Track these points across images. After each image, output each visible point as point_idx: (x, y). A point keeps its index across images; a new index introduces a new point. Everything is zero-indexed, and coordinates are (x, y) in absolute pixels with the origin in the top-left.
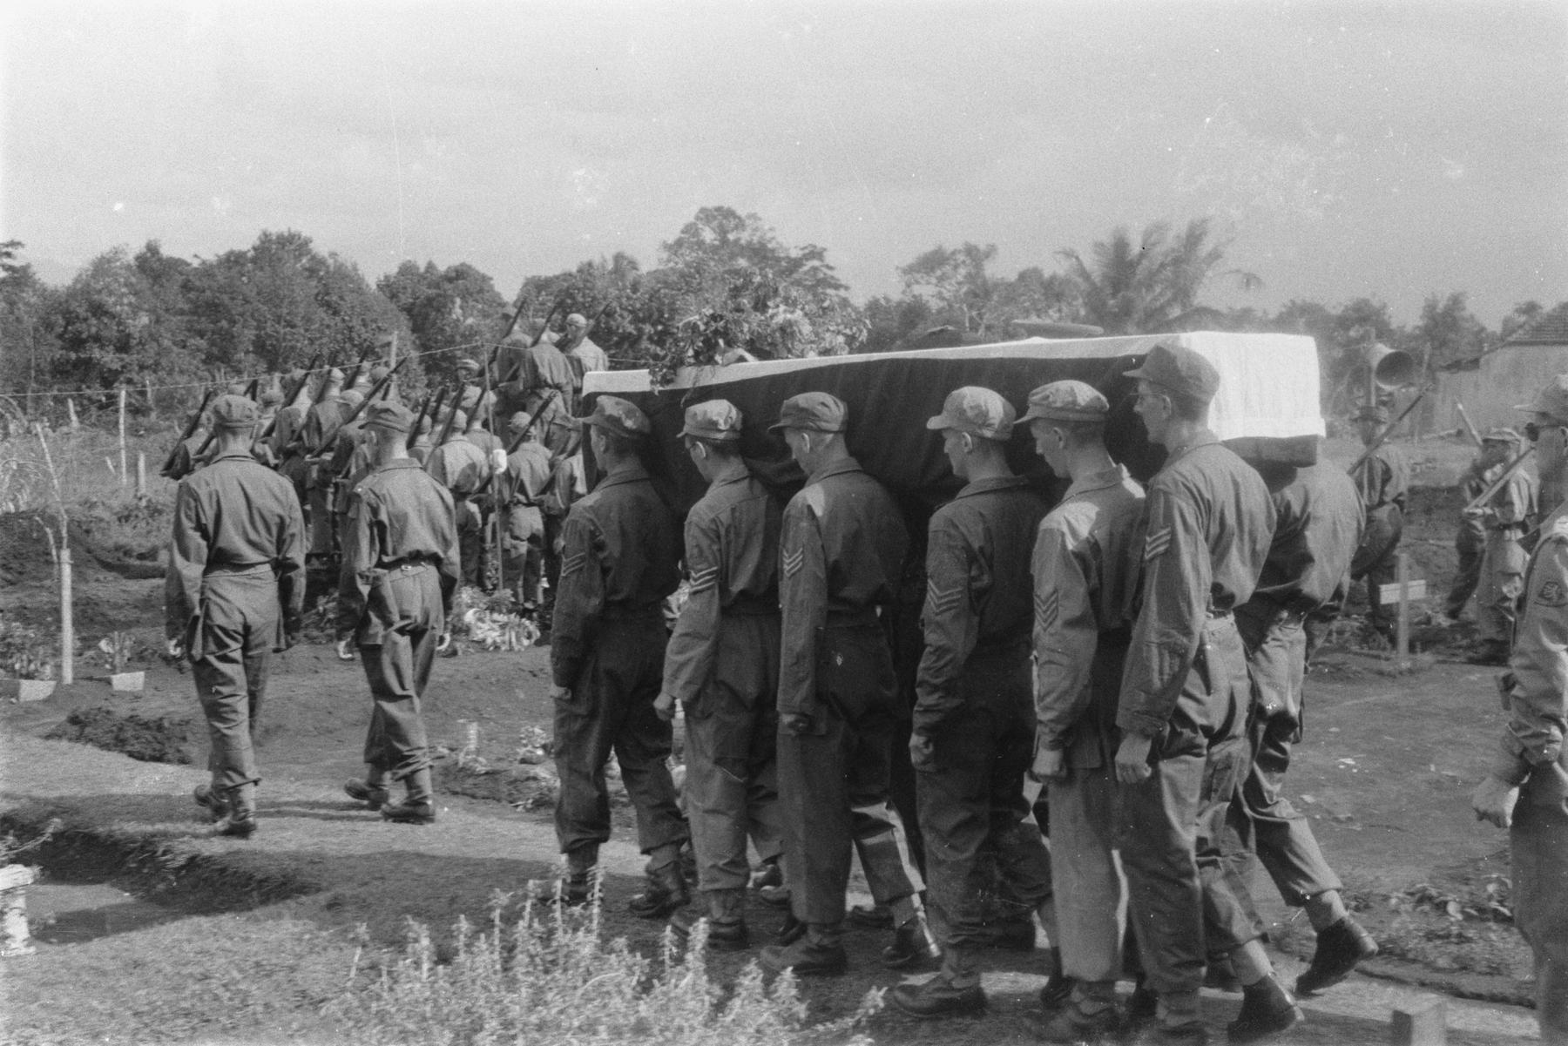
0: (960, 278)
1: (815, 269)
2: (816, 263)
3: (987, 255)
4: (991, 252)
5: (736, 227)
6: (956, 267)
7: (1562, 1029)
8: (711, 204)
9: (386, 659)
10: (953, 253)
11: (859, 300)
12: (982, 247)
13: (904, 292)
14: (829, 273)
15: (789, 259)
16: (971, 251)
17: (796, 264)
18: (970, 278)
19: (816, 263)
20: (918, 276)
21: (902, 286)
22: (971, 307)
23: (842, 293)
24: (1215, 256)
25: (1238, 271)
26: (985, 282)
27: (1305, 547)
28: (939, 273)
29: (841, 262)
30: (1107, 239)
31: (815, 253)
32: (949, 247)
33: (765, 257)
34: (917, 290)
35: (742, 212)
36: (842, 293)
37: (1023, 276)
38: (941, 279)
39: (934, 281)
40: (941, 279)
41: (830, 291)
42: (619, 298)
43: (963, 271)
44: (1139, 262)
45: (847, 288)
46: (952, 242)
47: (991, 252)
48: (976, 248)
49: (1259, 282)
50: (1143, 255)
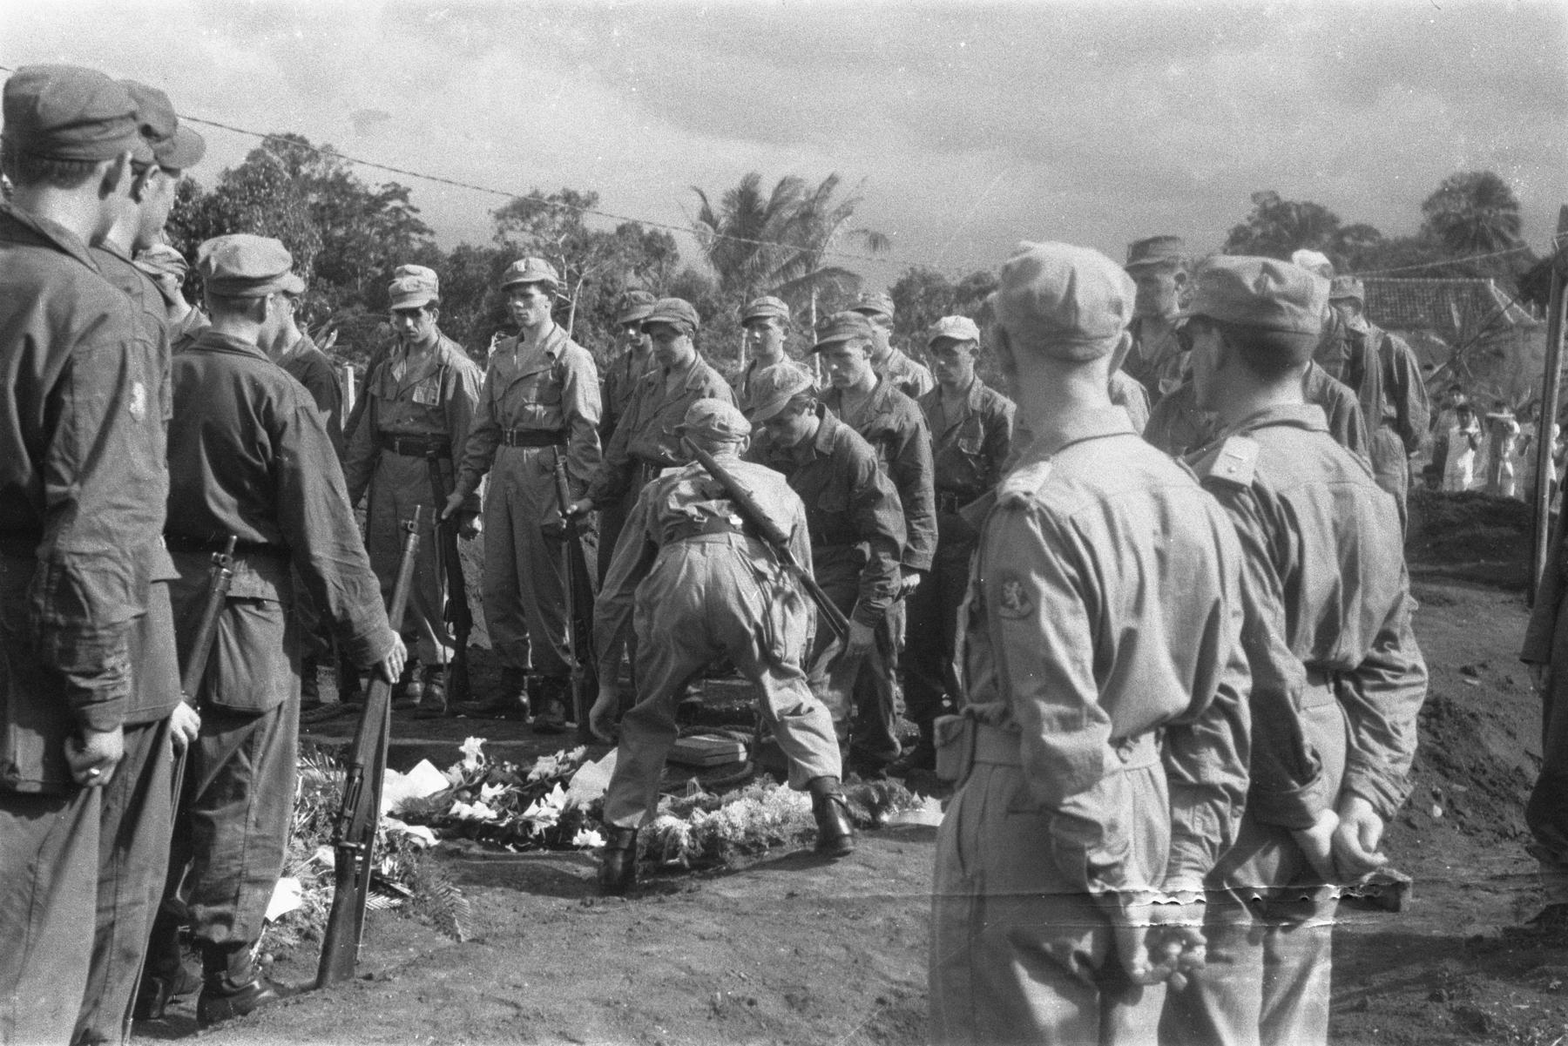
0: (557, 227)
1: (397, 210)
2: (397, 203)
3: (588, 203)
4: (591, 200)
5: (309, 158)
6: (554, 214)
7: (1335, 1033)
8: (282, 130)
9: (358, 772)
10: (552, 198)
11: (204, 193)
12: (582, 193)
13: (495, 239)
14: (414, 215)
15: (370, 197)
16: (569, 197)
17: (377, 202)
18: (569, 227)
19: (397, 203)
20: (511, 222)
21: (494, 233)
22: (568, 258)
23: (426, 237)
24: (845, 211)
25: (865, 231)
26: (585, 231)
27: (575, 403)
28: (535, 219)
29: (429, 204)
30: (735, 184)
31: (399, 193)
32: (547, 191)
33: (343, 192)
34: (510, 236)
35: (316, 142)
36: (426, 237)
37: (621, 230)
38: (537, 227)
39: (529, 228)
40: (537, 227)
41: (413, 235)
42: (836, 397)
43: (560, 218)
44: (768, 217)
45: (432, 233)
46: (550, 184)
47: (591, 200)
48: (575, 194)
49: (887, 243)
50: (775, 206)
